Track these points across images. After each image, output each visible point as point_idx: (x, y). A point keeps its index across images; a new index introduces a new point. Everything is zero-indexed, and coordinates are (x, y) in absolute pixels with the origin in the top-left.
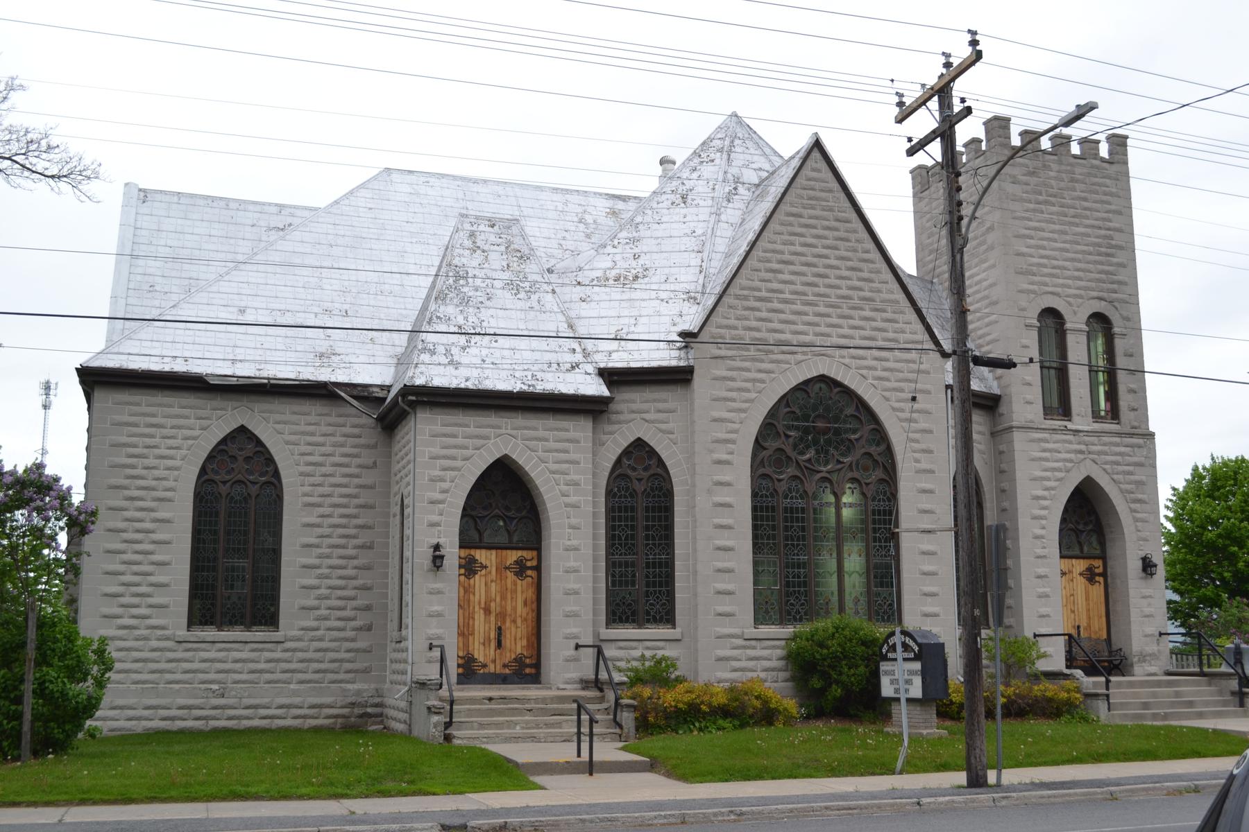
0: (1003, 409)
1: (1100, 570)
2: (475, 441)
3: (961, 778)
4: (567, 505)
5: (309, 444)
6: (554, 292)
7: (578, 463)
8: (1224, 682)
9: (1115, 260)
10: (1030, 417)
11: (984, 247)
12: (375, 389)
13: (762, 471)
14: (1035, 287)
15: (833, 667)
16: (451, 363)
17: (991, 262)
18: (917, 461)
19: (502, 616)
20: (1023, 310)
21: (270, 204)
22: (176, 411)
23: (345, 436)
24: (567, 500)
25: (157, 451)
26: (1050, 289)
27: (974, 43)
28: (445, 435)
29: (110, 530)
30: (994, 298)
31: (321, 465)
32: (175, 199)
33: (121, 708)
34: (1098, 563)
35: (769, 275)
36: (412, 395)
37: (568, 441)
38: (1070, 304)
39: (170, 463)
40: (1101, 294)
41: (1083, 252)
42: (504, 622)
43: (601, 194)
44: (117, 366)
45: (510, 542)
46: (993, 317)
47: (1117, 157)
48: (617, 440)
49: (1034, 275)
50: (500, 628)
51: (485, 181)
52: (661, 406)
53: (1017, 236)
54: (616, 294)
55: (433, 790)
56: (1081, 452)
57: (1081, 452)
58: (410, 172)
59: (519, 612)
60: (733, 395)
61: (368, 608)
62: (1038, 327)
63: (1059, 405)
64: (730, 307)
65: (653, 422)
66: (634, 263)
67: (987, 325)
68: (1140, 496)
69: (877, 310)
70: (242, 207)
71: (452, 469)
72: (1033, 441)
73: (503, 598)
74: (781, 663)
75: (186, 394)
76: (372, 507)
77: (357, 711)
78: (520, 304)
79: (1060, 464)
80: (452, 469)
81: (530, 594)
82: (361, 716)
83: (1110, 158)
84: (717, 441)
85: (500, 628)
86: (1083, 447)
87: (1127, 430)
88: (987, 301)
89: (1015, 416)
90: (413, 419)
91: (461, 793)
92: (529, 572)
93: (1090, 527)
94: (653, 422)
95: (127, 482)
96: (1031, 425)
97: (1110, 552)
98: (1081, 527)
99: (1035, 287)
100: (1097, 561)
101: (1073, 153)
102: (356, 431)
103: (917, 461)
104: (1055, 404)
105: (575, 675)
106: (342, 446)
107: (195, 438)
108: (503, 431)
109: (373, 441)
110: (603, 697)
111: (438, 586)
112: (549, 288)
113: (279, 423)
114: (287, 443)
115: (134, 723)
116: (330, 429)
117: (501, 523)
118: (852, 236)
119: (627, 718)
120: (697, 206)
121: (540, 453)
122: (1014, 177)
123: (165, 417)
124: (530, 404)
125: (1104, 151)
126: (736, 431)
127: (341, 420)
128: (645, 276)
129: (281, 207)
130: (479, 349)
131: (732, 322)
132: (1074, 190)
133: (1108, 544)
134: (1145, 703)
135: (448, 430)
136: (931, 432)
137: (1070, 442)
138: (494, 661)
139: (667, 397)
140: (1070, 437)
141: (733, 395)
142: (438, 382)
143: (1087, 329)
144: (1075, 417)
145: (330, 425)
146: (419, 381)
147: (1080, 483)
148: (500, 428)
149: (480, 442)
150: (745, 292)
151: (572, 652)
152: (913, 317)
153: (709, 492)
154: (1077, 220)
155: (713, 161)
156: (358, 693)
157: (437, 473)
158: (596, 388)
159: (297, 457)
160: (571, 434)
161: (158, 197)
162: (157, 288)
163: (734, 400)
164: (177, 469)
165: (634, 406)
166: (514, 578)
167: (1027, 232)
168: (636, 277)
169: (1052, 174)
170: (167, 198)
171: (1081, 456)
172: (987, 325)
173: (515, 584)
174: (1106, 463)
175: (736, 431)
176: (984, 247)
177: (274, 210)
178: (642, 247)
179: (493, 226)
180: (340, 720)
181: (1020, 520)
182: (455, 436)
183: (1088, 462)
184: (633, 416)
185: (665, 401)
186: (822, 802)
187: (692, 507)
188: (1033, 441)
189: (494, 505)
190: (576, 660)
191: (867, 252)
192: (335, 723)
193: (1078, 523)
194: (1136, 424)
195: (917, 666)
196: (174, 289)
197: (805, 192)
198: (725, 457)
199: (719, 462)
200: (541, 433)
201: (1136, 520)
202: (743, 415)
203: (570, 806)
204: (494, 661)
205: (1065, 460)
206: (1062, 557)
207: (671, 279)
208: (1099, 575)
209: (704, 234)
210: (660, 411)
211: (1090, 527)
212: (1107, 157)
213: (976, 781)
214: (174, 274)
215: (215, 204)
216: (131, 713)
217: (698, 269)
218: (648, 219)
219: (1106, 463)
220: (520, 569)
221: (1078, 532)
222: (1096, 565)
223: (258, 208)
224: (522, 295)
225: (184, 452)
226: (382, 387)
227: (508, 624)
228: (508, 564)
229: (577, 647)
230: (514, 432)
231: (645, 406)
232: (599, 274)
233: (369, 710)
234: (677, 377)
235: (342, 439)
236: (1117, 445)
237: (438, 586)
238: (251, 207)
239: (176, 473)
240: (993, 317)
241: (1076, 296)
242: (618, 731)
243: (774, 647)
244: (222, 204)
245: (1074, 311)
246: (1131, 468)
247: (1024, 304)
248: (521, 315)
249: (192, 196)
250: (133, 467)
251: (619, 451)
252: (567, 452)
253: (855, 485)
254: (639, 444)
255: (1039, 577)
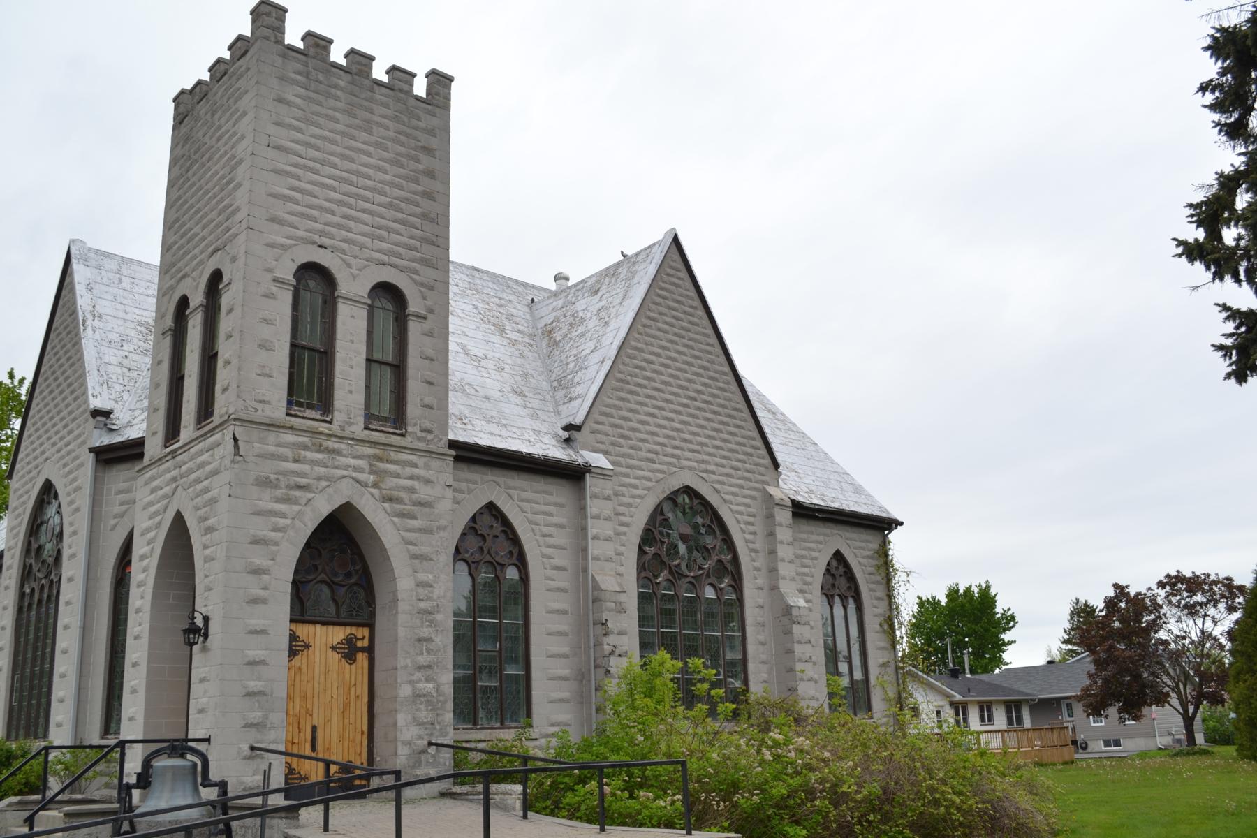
1: (366, 643)
13: (643, 574)
34: (363, 632)
47: (399, 84)
62: (294, 287)
83: (304, 49)
100: (361, 629)
101: (374, 77)
104: (386, 410)
125: (420, 88)
143: (369, 302)
147: (334, 511)
175: (627, 525)
189: (320, 568)
208: (363, 650)
212: (424, 96)
220: (349, 651)
222: (360, 636)
228: (335, 643)
245: (352, 274)
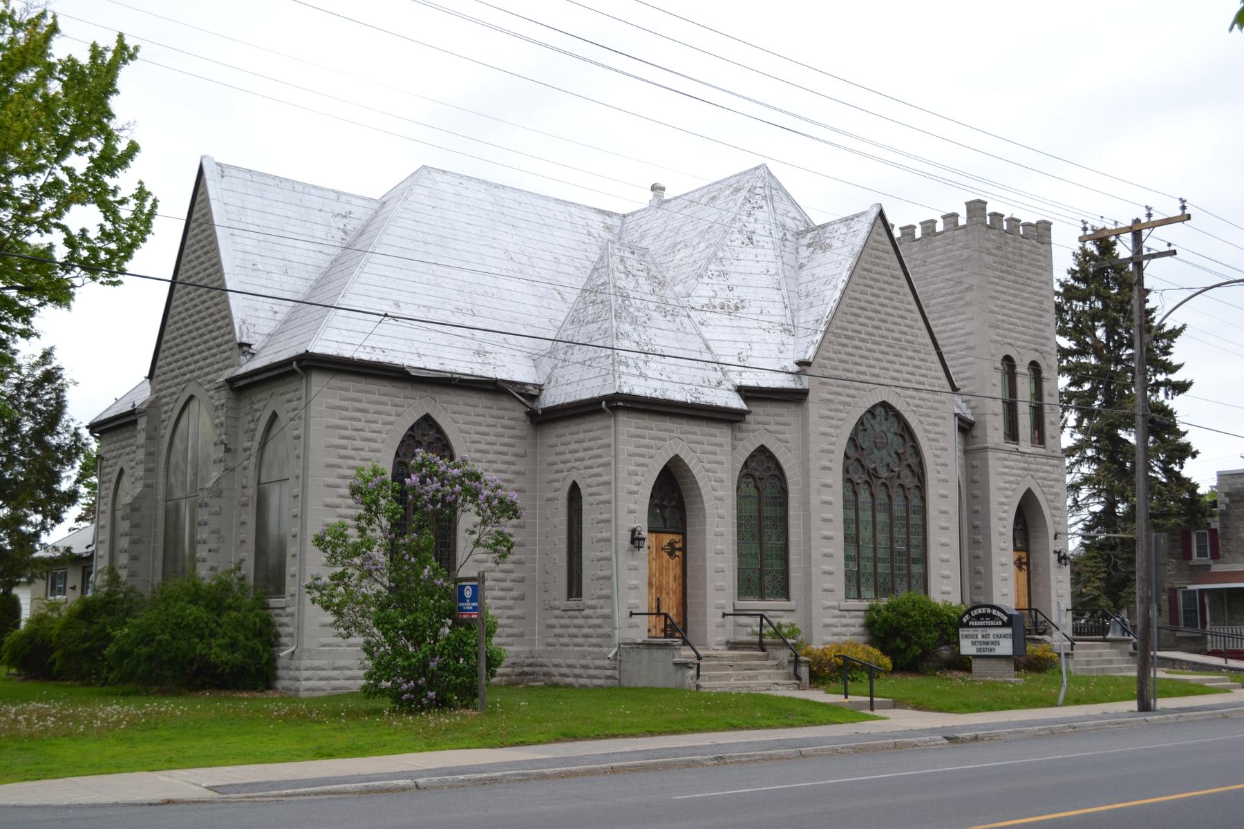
0: (977, 432)
2: (657, 442)
3: (1133, 705)
4: (716, 498)
5: (478, 433)
6: (689, 316)
7: (722, 463)
8: (1123, 646)
9: (1044, 320)
10: (997, 440)
11: (962, 303)
12: (530, 388)
14: (999, 338)
15: (913, 632)
16: (641, 375)
17: (969, 315)
18: (939, 472)
19: (660, 589)
20: (993, 356)
21: (328, 190)
22: (377, 397)
23: (504, 427)
24: (716, 494)
25: (363, 434)
26: (1009, 341)
27: (1184, 208)
28: (638, 436)
29: (328, 506)
30: (972, 344)
31: (487, 452)
32: (248, 176)
33: (340, 668)
35: (852, 318)
36: (621, 401)
37: (717, 445)
38: (1019, 353)
39: (373, 445)
40: (1036, 346)
41: (1027, 313)
42: (661, 594)
43: (590, 208)
44: (335, 353)
45: (665, 527)
46: (969, 360)
48: (748, 446)
49: (999, 328)
50: (658, 599)
51: (504, 187)
52: (779, 419)
53: (990, 297)
54: (724, 319)
55: (838, 720)
56: (1025, 469)
57: (1025, 469)
58: (444, 172)
59: (671, 584)
60: (832, 414)
61: (522, 580)
63: (1012, 433)
64: (830, 343)
65: (773, 432)
66: (731, 294)
67: (962, 365)
68: (1057, 504)
69: (916, 351)
70: (306, 190)
71: (642, 465)
72: (999, 459)
73: (661, 574)
74: (860, 630)
75: (385, 383)
76: (524, 491)
77: (518, 670)
78: (671, 326)
79: (1013, 478)
80: (642, 465)
81: (678, 571)
82: (519, 675)
84: (823, 451)
85: (658, 599)
86: (1026, 465)
87: (1050, 453)
88: (963, 346)
89: (989, 439)
90: (304, 385)
91: (854, 722)
92: (677, 553)
93: (674, 503)
94: (773, 432)
95: (340, 461)
96: (998, 447)
97: (1032, 547)
98: (665, 503)
99: (999, 338)
102: (512, 423)
103: (939, 472)
105: (722, 639)
106: (502, 436)
107: (391, 424)
108: (675, 435)
109: (524, 433)
110: (768, 655)
111: (635, 563)
112: (685, 313)
113: (455, 413)
114: (462, 431)
115: (351, 682)
116: (493, 421)
117: (658, 511)
118: (901, 290)
119: (804, 671)
120: (763, 247)
121: (699, 454)
122: (988, 249)
123: (369, 403)
124: (719, 416)
126: (833, 444)
127: (500, 413)
128: (743, 307)
129: (339, 194)
130: (654, 367)
131: (831, 355)
132: (1021, 262)
133: (1031, 540)
134: (1087, 661)
135: (640, 432)
136: (946, 450)
137: (1019, 461)
138: (655, 627)
139: (785, 413)
140: (1019, 458)
141: (832, 414)
142: (638, 391)
144: (1021, 442)
145: (493, 417)
146: (626, 390)
148: (672, 431)
149: (660, 443)
150: (839, 331)
151: (720, 620)
152: (936, 358)
153: (819, 492)
154: (1023, 287)
155: (761, 207)
156: (518, 654)
157: (633, 468)
158: (736, 403)
159: (469, 445)
160: (718, 440)
161: (234, 173)
162: (260, 267)
163: (832, 418)
164: (378, 451)
165: (760, 419)
166: (668, 557)
167: (996, 294)
168: (737, 308)
169: (1010, 249)
170: (241, 175)
171: (1026, 473)
172: (962, 365)
173: (668, 562)
174: (1039, 478)
176: (962, 303)
177: (289, 185)
178: (733, 280)
179: (633, 253)
180: (504, 678)
181: (992, 521)
182: (644, 437)
183: (1029, 477)
184: (760, 426)
185: (782, 416)
186: (291, 788)
187: (806, 503)
188: (999, 459)
190: (723, 626)
191: (910, 304)
192: (501, 681)
193: (662, 499)
194: (1054, 449)
195: (1009, 631)
196: (274, 269)
197: (872, 252)
198: (828, 464)
199: (825, 468)
200: (699, 438)
201: (1055, 523)
202: (838, 431)
203: (986, 724)
204: (655, 627)
205: (1017, 475)
206: (1015, 550)
207: (765, 312)
209: (777, 274)
210: (778, 424)
211: (674, 503)
213: (1145, 707)
214: (268, 253)
215: (283, 185)
216: (323, 673)
217: (783, 306)
218: (728, 255)
219: (1039, 478)
220: (671, 550)
221: (662, 508)
223: (320, 193)
224: (669, 318)
225: (384, 436)
226: (535, 385)
227: (664, 595)
229: (724, 615)
230: (681, 436)
231: (767, 419)
232: (706, 301)
233: (526, 669)
234: (794, 397)
235: (502, 430)
236: (1045, 464)
237: (635, 563)
238: (314, 191)
239: (378, 454)
240: (969, 360)
241: (1024, 347)
242: (798, 682)
243: (857, 617)
244: (289, 185)
246: (1052, 483)
247: (993, 351)
248: (671, 335)
249: (262, 175)
250: (345, 448)
251: (748, 455)
252: (715, 454)
253: (750, 480)
254: (762, 450)
255: (943, 561)
